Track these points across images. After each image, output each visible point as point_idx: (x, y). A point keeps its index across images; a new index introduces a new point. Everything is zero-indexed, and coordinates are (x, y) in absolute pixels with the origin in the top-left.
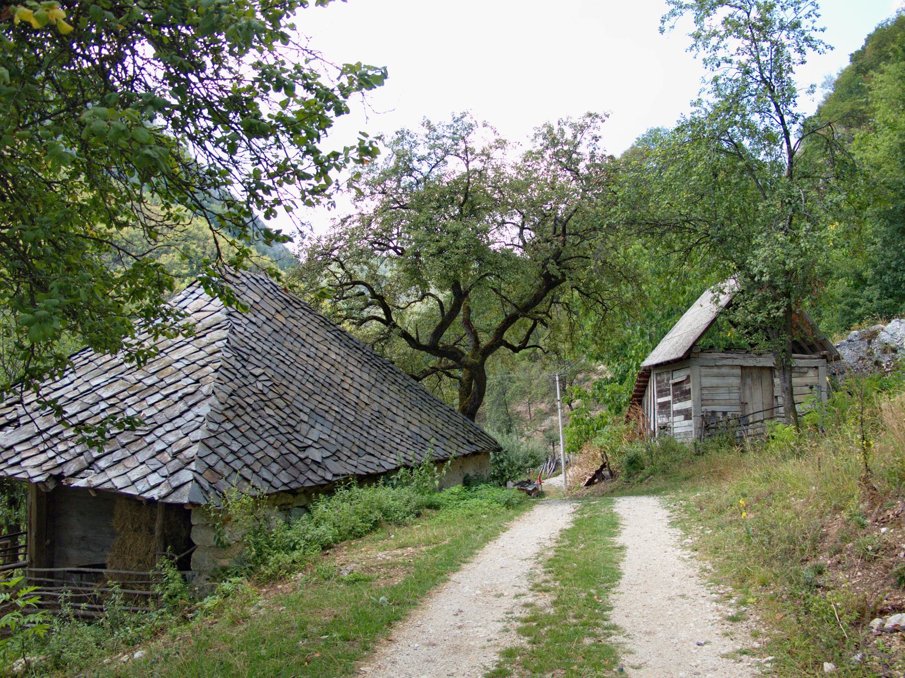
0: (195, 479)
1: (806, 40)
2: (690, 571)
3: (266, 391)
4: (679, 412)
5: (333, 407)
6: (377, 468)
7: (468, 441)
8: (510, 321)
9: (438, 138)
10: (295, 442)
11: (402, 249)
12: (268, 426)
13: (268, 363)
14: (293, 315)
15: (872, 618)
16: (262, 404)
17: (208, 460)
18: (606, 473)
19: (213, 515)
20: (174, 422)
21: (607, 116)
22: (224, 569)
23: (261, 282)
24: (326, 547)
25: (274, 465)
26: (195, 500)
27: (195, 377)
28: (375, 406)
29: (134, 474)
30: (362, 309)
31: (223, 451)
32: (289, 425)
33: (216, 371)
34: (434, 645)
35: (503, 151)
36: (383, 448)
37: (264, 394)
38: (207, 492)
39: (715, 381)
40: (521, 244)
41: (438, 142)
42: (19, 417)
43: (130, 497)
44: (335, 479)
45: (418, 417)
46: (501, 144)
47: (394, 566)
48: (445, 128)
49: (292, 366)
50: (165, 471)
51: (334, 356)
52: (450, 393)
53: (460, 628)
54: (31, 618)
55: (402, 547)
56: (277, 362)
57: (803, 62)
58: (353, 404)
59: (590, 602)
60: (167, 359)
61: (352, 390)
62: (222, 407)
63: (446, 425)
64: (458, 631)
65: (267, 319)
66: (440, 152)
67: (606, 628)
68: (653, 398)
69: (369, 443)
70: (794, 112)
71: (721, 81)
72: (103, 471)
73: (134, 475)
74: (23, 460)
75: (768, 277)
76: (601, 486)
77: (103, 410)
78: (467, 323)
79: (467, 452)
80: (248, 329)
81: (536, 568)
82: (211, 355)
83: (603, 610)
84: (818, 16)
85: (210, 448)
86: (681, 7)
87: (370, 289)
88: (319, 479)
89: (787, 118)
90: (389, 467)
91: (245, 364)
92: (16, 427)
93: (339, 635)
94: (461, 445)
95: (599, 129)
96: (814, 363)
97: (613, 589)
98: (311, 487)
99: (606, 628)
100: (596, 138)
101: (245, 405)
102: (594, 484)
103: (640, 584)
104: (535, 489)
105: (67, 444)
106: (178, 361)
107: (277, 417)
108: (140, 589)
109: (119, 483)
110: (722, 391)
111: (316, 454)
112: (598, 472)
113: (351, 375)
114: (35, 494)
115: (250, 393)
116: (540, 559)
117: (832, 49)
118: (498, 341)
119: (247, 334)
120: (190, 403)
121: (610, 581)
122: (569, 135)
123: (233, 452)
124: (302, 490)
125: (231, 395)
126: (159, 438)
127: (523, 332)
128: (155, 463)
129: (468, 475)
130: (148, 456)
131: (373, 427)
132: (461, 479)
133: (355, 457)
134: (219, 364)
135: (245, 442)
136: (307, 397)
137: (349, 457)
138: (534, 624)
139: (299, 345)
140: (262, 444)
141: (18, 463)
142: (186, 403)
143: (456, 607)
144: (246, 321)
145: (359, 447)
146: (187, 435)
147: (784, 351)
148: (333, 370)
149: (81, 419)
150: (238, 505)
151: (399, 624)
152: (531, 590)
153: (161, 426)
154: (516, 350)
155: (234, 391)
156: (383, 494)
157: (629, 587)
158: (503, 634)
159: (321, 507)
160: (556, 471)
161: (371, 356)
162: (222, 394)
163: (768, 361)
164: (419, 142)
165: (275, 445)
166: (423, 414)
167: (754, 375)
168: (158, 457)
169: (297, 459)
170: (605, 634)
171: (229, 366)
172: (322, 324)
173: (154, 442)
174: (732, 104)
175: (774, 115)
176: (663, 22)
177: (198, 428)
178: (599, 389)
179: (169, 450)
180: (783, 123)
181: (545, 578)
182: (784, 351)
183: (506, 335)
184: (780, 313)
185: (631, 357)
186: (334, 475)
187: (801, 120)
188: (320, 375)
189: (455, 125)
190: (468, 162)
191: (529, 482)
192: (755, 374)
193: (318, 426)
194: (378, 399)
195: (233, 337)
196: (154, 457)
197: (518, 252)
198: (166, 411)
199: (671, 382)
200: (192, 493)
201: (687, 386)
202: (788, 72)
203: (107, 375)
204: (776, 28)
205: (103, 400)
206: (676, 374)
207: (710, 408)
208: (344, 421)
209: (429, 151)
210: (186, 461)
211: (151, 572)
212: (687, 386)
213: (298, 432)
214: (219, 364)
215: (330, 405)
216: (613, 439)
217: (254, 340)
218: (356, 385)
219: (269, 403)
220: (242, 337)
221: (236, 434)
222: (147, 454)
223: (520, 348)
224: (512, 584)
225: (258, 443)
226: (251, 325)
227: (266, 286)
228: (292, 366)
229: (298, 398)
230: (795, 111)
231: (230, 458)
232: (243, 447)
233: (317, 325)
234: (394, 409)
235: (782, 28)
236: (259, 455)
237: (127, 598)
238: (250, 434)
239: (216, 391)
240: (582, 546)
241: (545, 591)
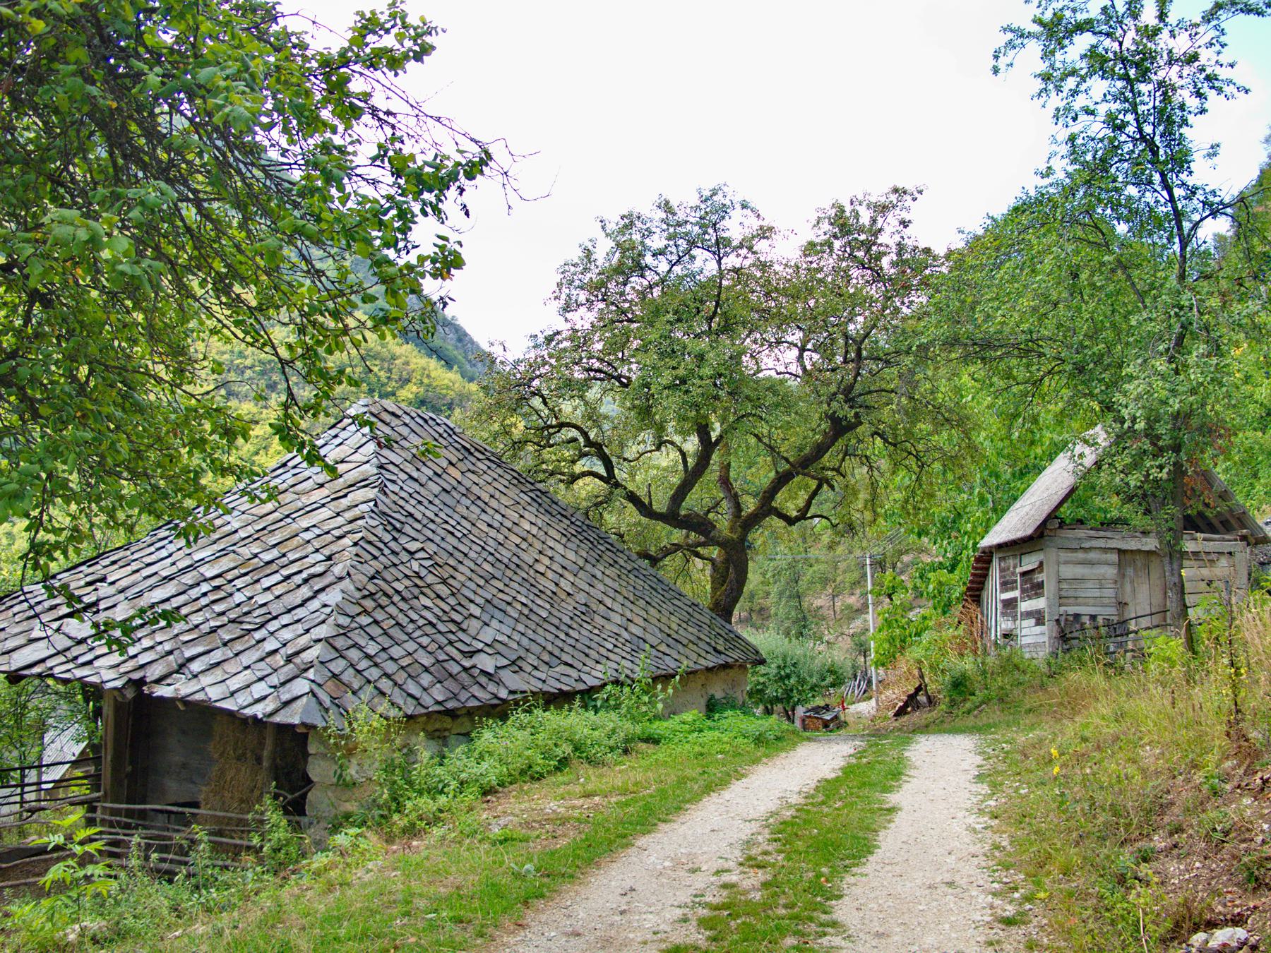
0: (312, 691)
1: (1208, 78)
3: (423, 572)
4: (1028, 614)
5: (520, 597)
6: (574, 684)
7: (715, 649)
8: (782, 480)
9: (679, 225)
10: (459, 645)
11: (629, 378)
13: (430, 534)
16: (416, 591)
17: (332, 666)
18: (922, 698)
19: (332, 741)
21: (920, 192)
22: (347, 816)
23: (430, 422)
24: (487, 792)
26: (308, 721)
27: (327, 552)
28: (582, 598)
30: (574, 462)
31: (354, 654)
32: (453, 621)
33: (356, 544)
34: (578, 935)
35: (769, 242)
36: (587, 655)
37: (421, 578)
38: (327, 710)
39: (1079, 571)
40: (800, 372)
41: (679, 230)
42: (99, 600)
43: (230, 713)
44: (511, 697)
45: (644, 614)
46: (765, 233)
47: (564, 821)
48: (688, 211)
49: (464, 540)
50: (274, 680)
51: (527, 526)
52: (699, 578)
53: (622, 913)
55: (587, 795)
56: (443, 533)
57: (1203, 111)
58: (549, 593)
59: (815, 888)
60: (294, 526)
61: (550, 574)
62: (358, 595)
63: (684, 625)
64: (618, 918)
65: (435, 473)
66: (683, 244)
67: (822, 925)
68: (995, 594)
69: (567, 648)
70: (1190, 183)
71: (1079, 141)
72: (195, 676)
73: (234, 684)
74: (97, 658)
75: (1143, 424)
76: (915, 717)
77: (205, 594)
78: (725, 482)
79: (711, 665)
80: (405, 488)
81: (759, 834)
82: (351, 522)
83: (828, 899)
84: (1222, 46)
85: (336, 650)
86: (1022, 36)
87: (585, 434)
88: (489, 696)
89: (1178, 192)
91: (397, 535)
92: (95, 613)
93: (451, 914)
94: (703, 654)
95: (908, 210)
96: (1227, 547)
97: (854, 870)
98: (478, 708)
99: (822, 925)
100: (905, 224)
101: (391, 592)
102: (906, 713)
103: (896, 864)
104: (836, 717)
105: (153, 639)
106: (307, 529)
107: (436, 610)
108: (241, 838)
109: (214, 693)
110: (1089, 584)
112: (912, 698)
113: (550, 553)
115: (400, 576)
116: (771, 820)
117: (1247, 92)
118: (767, 508)
119: (403, 494)
120: (316, 588)
121: (854, 857)
122: (865, 219)
123: (368, 656)
124: (464, 711)
125: (373, 578)
126: (272, 633)
127: (803, 496)
128: (263, 668)
129: (713, 697)
130: (255, 658)
131: (575, 626)
132: (703, 702)
133: (544, 668)
134: (360, 535)
135: (386, 642)
136: (482, 582)
137: (536, 668)
138: (726, 913)
139: (478, 511)
140: (411, 646)
141: (90, 662)
143: (628, 884)
144: (404, 477)
145: (551, 653)
147: (1170, 529)
148: (524, 546)
150: (365, 729)
151: (541, 904)
152: (741, 864)
153: (276, 618)
154: (791, 521)
155: (378, 572)
156: (577, 722)
157: (878, 868)
158: (677, 926)
159: (487, 735)
160: (866, 695)
161: (584, 527)
163: (1151, 543)
164: (654, 230)
165: (429, 649)
166: (652, 611)
167: (1139, 564)
168: (268, 660)
169: (460, 669)
170: (816, 933)
171: (373, 538)
172: (515, 482)
174: (1095, 172)
175: (1159, 188)
176: (996, 57)
177: (323, 622)
178: (921, 577)
179: (282, 651)
180: (1172, 199)
182: (1170, 529)
183: (780, 496)
184: (1164, 475)
185: (965, 533)
186: (511, 692)
187: (1200, 195)
188: (504, 552)
189: (703, 206)
190: (720, 259)
191: (827, 708)
192: (1140, 561)
193: (494, 623)
194: (587, 588)
195: (383, 498)
196: (262, 659)
197: (793, 383)
198: (284, 597)
199: (1019, 570)
200: (306, 710)
201: (1039, 577)
202: (1180, 126)
203: (216, 547)
204: (1161, 63)
205: (206, 580)
206: (1026, 559)
207: (1072, 610)
208: (533, 617)
210: (303, 667)
211: (250, 816)
212: (1039, 577)
213: (464, 631)
214: (360, 535)
216: (938, 648)
217: (413, 502)
218: (555, 567)
219: (426, 590)
220: (396, 498)
221: (375, 631)
223: (797, 519)
224: (719, 854)
225: (406, 645)
227: (437, 428)
228: (464, 540)
229: (469, 584)
230: (1191, 181)
231: (363, 664)
232: (384, 649)
233: (507, 483)
234: (609, 602)
235: (1170, 63)
236: (404, 662)
238: (396, 632)
239: (352, 571)
241: (759, 867)
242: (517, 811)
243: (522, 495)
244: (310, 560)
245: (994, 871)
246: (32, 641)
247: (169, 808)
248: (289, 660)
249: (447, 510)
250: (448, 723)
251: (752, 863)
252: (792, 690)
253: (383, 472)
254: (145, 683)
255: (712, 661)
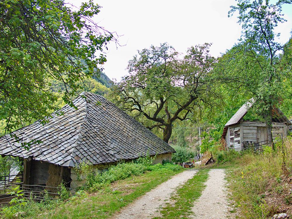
0: (72, 159)
1: (278, 18)
2: (224, 195)
4: (236, 141)
5: (119, 137)
7: (164, 149)
8: (180, 110)
10: (105, 148)
12: (97, 143)
13: (99, 123)
14: (109, 108)
15: (275, 214)
16: (96, 136)
17: (76, 153)
18: (212, 160)
19: (76, 170)
20: (67, 141)
21: (211, 44)
22: (80, 187)
23: (99, 97)
24: (112, 182)
25: (98, 155)
27: (75, 127)
28: (134, 137)
29: (54, 157)
30: (132, 106)
31: (81, 150)
32: (104, 143)
33: (82, 125)
36: (135, 151)
37: (97, 133)
38: (75, 163)
40: (184, 86)
44: (118, 160)
46: (176, 54)
47: (130, 189)
48: (158, 48)
50: (63, 156)
52: (161, 133)
54: (21, 200)
56: (102, 123)
57: (276, 26)
59: (187, 204)
60: (68, 121)
61: (126, 132)
62: (82, 137)
63: (157, 144)
65: (100, 109)
68: (229, 136)
70: (273, 42)
71: (248, 32)
72: (45, 155)
73: (54, 157)
74: (22, 151)
76: (210, 165)
77: (47, 137)
80: (93, 112)
81: (174, 192)
82: (81, 120)
83: (190, 207)
87: (134, 100)
88: (112, 160)
89: (271, 44)
90: (136, 157)
92: (22, 141)
94: (162, 150)
95: (209, 48)
96: (282, 126)
99: (189, 213)
100: (208, 51)
101: (90, 136)
103: (206, 198)
105: (35, 147)
106: (71, 122)
107: (100, 140)
108: (55, 193)
109: (49, 159)
110: (250, 134)
111: (112, 152)
112: (209, 160)
113: (126, 127)
114: (26, 161)
116: (177, 188)
117: (286, 21)
118: (176, 117)
119: (93, 114)
120: (73, 135)
121: (196, 197)
122: (199, 50)
123: (85, 151)
124: (107, 163)
125: (86, 133)
126: (62, 146)
127: (185, 114)
128: (60, 154)
129: (164, 160)
130: (58, 151)
131: (132, 144)
132: (162, 161)
133: (125, 153)
134: (83, 123)
136: (111, 134)
137: (123, 153)
139: (110, 117)
140: (94, 148)
141: (21, 152)
142: (72, 135)
146: (71, 145)
147: (269, 122)
148: (120, 125)
149: (40, 139)
152: (170, 199)
153: (63, 142)
154: (182, 120)
156: (132, 166)
159: (112, 169)
160: (199, 160)
161: (134, 121)
162: (83, 133)
163: (264, 125)
165: (99, 149)
168: (61, 152)
169: (106, 154)
170: (188, 214)
172: (118, 111)
173: (61, 147)
174: (251, 39)
175: (266, 43)
177: (74, 143)
180: (269, 46)
181: (176, 195)
184: (267, 109)
186: (118, 159)
187: (276, 45)
188: (116, 127)
189: (161, 47)
190: (166, 59)
191: (190, 163)
193: (114, 143)
194: (135, 135)
195: (88, 114)
196: (60, 152)
197: (182, 88)
198: (65, 137)
199: (234, 131)
200: (70, 163)
201: (239, 133)
202: (271, 29)
204: (267, 14)
205: (47, 133)
206: (236, 128)
207: (246, 140)
209: (153, 56)
211: (57, 188)
212: (239, 133)
213: (107, 145)
214: (83, 123)
215: (118, 136)
216: (216, 149)
217: (95, 115)
220: (91, 114)
221: (86, 145)
222: (59, 150)
223: (183, 119)
224: (165, 196)
225: (93, 148)
226: (94, 111)
232: (88, 149)
233: (116, 111)
237: (50, 195)
238: (91, 145)
239: (81, 131)
240: (193, 185)
241: (174, 199)
242: (119, 186)
243: (120, 114)
244: (71, 129)
245: (228, 200)
246: (7, 147)
247: (39, 186)
248: (66, 152)
249: (102, 117)
250: (103, 166)
251: (173, 198)
252: (182, 159)
253: (88, 108)
254: (33, 157)
255: (164, 152)
